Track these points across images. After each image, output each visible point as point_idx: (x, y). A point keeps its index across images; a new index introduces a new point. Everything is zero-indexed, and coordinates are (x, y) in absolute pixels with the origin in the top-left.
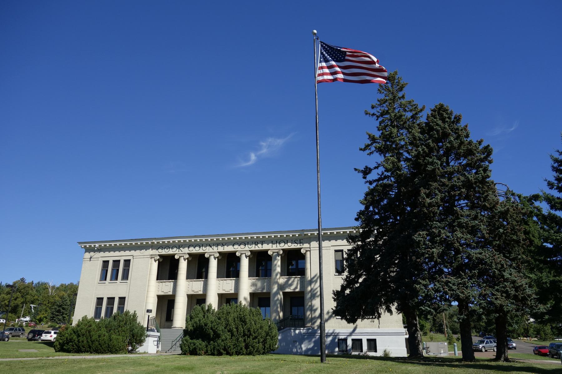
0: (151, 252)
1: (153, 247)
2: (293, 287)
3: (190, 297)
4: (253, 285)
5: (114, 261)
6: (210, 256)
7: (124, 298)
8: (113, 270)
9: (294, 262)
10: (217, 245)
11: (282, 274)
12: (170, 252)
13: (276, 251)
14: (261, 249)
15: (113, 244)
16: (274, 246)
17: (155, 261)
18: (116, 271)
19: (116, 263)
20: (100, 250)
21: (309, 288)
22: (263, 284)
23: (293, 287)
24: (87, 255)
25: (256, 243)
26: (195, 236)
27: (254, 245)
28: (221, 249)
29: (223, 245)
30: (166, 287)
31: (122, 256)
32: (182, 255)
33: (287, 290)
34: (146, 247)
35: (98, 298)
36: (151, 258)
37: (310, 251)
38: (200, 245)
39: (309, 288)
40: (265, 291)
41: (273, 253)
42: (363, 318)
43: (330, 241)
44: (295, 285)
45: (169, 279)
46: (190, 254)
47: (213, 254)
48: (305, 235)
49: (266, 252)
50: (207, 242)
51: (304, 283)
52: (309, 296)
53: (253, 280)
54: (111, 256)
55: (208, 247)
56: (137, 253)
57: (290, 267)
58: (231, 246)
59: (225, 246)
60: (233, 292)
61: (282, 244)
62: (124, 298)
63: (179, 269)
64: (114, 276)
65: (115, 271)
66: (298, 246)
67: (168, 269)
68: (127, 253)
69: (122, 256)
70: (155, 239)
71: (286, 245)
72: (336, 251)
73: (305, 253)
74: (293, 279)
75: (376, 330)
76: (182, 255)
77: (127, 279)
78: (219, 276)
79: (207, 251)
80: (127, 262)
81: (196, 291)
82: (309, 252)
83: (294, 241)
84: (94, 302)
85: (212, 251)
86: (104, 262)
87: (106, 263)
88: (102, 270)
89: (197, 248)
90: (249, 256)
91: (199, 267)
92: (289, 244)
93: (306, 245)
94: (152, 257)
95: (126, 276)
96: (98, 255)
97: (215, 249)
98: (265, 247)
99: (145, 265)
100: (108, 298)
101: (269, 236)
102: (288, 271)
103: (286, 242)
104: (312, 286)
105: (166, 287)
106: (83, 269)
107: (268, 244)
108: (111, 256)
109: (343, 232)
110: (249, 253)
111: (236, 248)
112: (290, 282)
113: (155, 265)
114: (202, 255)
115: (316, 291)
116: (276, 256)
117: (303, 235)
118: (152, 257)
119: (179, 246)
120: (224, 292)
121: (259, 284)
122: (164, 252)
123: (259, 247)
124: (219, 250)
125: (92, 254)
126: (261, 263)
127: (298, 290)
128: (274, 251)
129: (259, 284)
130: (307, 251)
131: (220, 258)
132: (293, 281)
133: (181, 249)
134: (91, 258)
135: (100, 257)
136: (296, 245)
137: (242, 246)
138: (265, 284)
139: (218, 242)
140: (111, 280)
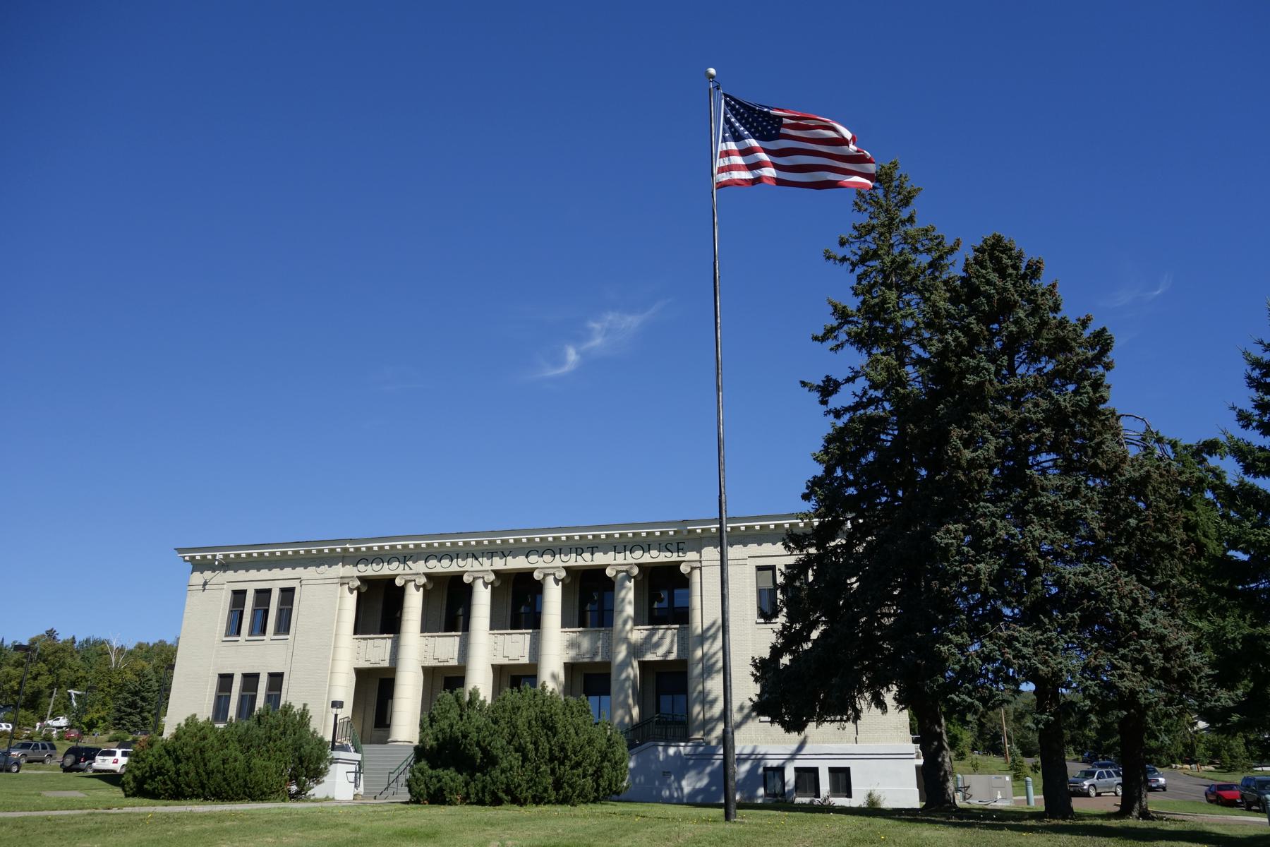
0: (340, 570)
2: (661, 651)
4: (573, 645)
6: (475, 579)
7: (281, 675)
8: (254, 611)
9: (665, 593)
10: (491, 554)
11: (637, 621)
12: (385, 570)
13: (624, 568)
16: (620, 558)
17: (351, 591)
18: (263, 614)
19: (263, 595)
20: (226, 566)
21: (699, 653)
22: (594, 642)
23: (661, 651)
24: (197, 578)
25: (579, 551)
27: (574, 555)
28: (499, 564)
29: (504, 555)
30: (376, 651)
31: (275, 579)
32: (412, 578)
33: (650, 657)
34: (330, 560)
35: (221, 676)
36: (342, 584)
37: (700, 568)
38: (452, 555)
39: (699, 653)
40: (598, 659)
41: (618, 572)
44: (666, 645)
45: (382, 633)
46: (429, 576)
47: (480, 575)
48: (689, 531)
49: (601, 570)
50: (467, 548)
51: (686, 641)
52: (698, 670)
53: (573, 633)
54: (252, 580)
55: (470, 560)
56: (311, 572)
58: (522, 558)
59: (509, 558)
61: (638, 553)
62: (281, 675)
64: (258, 624)
65: (260, 614)
66: (674, 557)
67: (379, 608)
68: (288, 572)
69: (275, 579)
71: (646, 554)
72: (759, 568)
73: (690, 573)
75: (850, 747)
76: (412, 578)
77: (287, 631)
79: (468, 567)
80: (288, 594)
81: (442, 658)
83: (665, 546)
86: (235, 592)
87: (239, 596)
88: (231, 611)
89: (446, 562)
90: (562, 580)
91: (449, 605)
92: (654, 553)
93: (692, 556)
94: (343, 581)
95: (284, 626)
96: (221, 577)
98: (600, 559)
99: (328, 601)
100: (245, 675)
103: (646, 548)
104: (706, 647)
105: (376, 651)
107: (605, 553)
108: (252, 580)
110: (563, 574)
111: (534, 562)
112: (655, 638)
113: (351, 601)
114: (456, 578)
115: (713, 660)
117: (685, 533)
118: (343, 581)
119: (405, 557)
121: (585, 643)
122: (372, 570)
123: (586, 560)
124: (496, 567)
125: (208, 574)
126: (590, 596)
127: (673, 657)
128: (620, 568)
129: (585, 643)
130: (693, 568)
131: (497, 584)
132: (663, 637)
133: (410, 563)
134: (205, 584)
135: (226, 582)
136: (669, 554)
137: (547, 558)
138: (600, 643)
139: (493, 547)
140: (251, 634)
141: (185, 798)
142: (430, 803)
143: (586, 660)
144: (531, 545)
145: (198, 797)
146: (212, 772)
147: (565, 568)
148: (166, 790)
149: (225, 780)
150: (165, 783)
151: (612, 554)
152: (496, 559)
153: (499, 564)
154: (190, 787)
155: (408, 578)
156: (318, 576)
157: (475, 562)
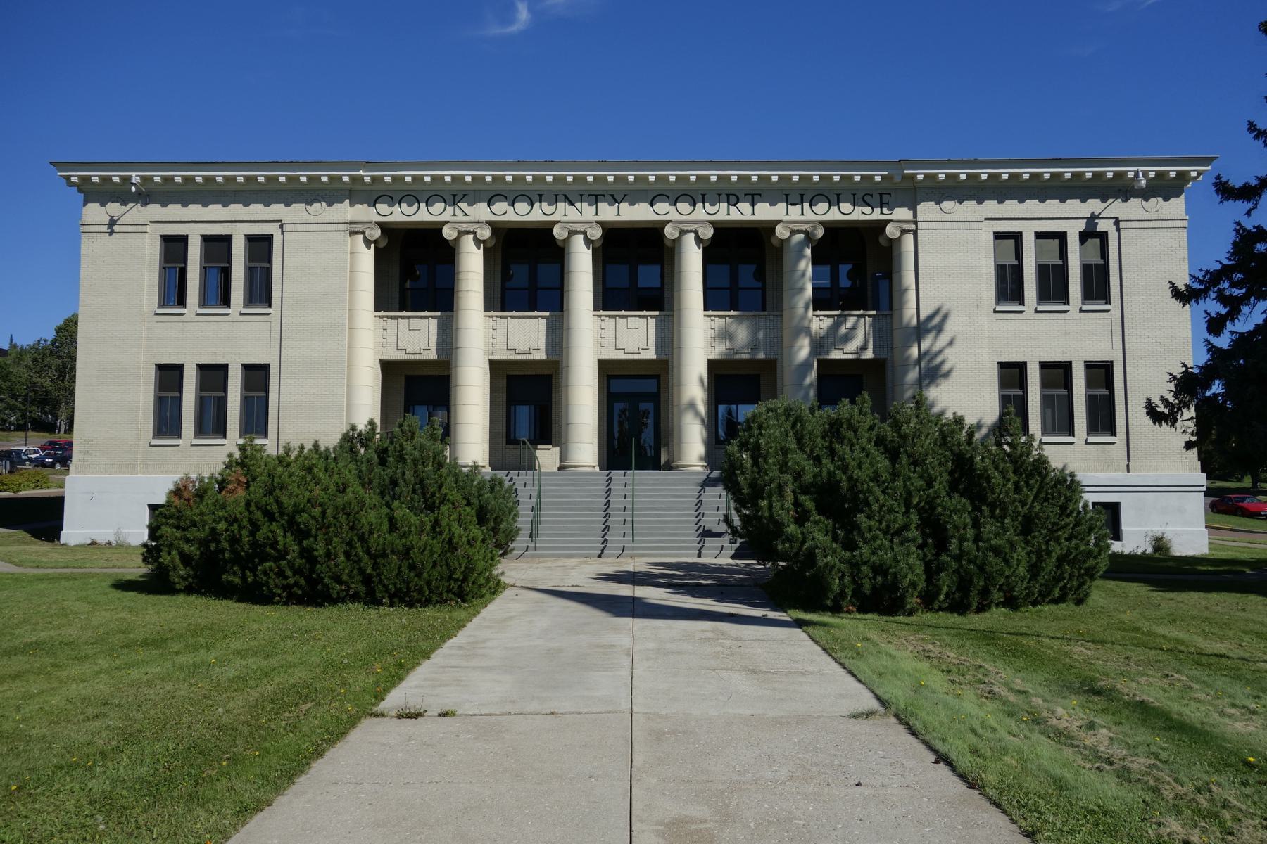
0: (346, 211)
1: (357, 193)
2: (852, 346)
3: (610, 372)
4: (725, 335)
5: (206, 239)
6: (461, 234)
7: (265, 368)
8: (205, 270)
9: (861, 267)
10: (595, 198)
11: (820, 303)
12: (423, 214)
13: (803, 227)
14: (749, 218)
15: (199, 176)
16: (795, 212)
17: (367, 243)
18: (233, 274)
19: (217, 246)
20: (146, 196)
21: (914, 352)
22: (755, 331)
23: (852, 346)
24: (95, 213)
25: (732, 198)
26: (520, 164)
27: (724, 205)
28: (608, 213)
29: (614, 200)
30: (416, 336)
31: (239, 221)
32: (469, 227)
33: (836, 354)
34: (332, 194)
35: (161, 368)
36: (353, 233)
37: (915, 233)
38: (533, 197)
39: (914, 352)
40: (761, 356)
41: (793, 232)
42: (351, 440)
43: (980, 202)
44: (857, 338)
45: (503, 310)
46: (495, 227)
47: (581, 228)
48: (905, 177)
49: (768, 228)
50: (559, 187)
51: (886, 330)
52: (913, 375)
53: (719, 320)
54: (196, 222)
55: (561, 205)
56: (296, 212)
57: (408, 285)
58: (483, 206)
59: (624, 205)
60: (432, 355)
61: (822, 207)
62: (265, 368)
63: (462, 276)
64: (215, 292)
65: (215, 277)
66: (876, 215)
67: (414, 271)
68: (257, 211)
69: (239, 221)
70: (367, 165)
71: (834, 209)
72: (999, 236)
73: (457, 240)
74: (851, 321)
75: (1120, 477)
76: (469, 227)
77: (268, 302)
78: (491, 303)
79: (561, 215)
80: (261, 246)
81: (521, 348)
82: (910, 237)
83: (862, 196)
84: (991, 379)
85: (578, 217)
86: (166, 239)
87: (174, 247)
88: (164, 269)
89: (522, 207)
90: (375, 242)
91: (526, 268)
92: (846, 207)
93: (902, 213)
94: (354, 229)
95: (260, 292)
96: (136, 213)
97: (481, 211)
98: (764, 212)
99: (329, 259)
100: (202, 368)
101: (353, 178)
102: (503, 297)
103: (834, 199)
104: (925, 344)
105: (416, 336)
106: (85, 262)
107: (773, 204)
108: (196, 222)
109: (1073, 174)
110: (376, 233)
111: (662, 211)
112: (843, 330)
113: (366, 259)
114: (432, 232)
115: (938, 360)
116: (802, 245)
117: (898, 179)
118: (354, 229)
119: (454, 195)
120: (401, 356)
121: (742, 334)
122: (400, 214)
123: (743, 213)
124: (601, 218)
125: (114, 208)
126: (743, 264)
127: (869, 354)
128: (796, 227)
129: (742, 334)
130: (904, 232)
131: (383, 244)
132: (854, 328)
133: (463, 205)
134: (112, 223)
135: (148, 225)
136: (867, 210)
137: (684, 207)
138: (761, 335)
139: (599, 187)
140: (204, 303)
141: (334, 601)
142: (860, 611)
143: (745, 356)
144: (437, 186)
145: (355, 598)
146: (384, 554)
147: (380, 224)
148: (286, 588)
149: (412, 567)
150: (281, 574)
151: (782, 206)
152: (603, 206)
153: (608, 213)
154: (340, 582)
155: (463, 227)
156: (940, 216)
157: (570, 209)
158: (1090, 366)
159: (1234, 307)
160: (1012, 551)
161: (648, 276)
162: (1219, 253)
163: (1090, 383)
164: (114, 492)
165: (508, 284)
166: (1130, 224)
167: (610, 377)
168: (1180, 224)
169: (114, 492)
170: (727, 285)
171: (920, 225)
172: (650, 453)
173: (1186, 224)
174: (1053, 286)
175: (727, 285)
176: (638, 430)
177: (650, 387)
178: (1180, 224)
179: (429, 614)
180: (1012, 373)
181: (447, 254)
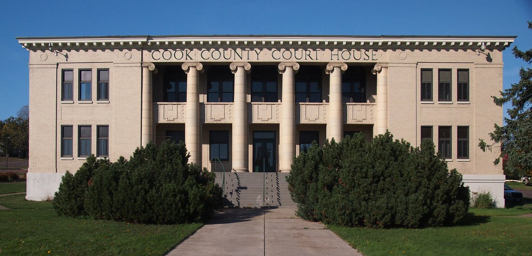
54: (437, 60)
106: (31, 81)
108: (437, 60)
109: (347, 43)
158: (441, 128)
159: (520, 104)
160: (94, 187)
161: (270, 86)
162: (517, 80)
163: (459, 136)
164: (43, 182)
165: (210, 91)
166: (136, 65)
167: (254, 132)
168: (500, 66)
169: (43, 182)
170: (218, 91)
171: (140, 65)
172: (271, 165)
173: (502, 66)
174: (445, 94)
175: (218, 91)
176: (267, 156)
177: (270, 136)
178: (500, 66)
179: (178, 227)
180: (426, 131)
181: (278, 78)
